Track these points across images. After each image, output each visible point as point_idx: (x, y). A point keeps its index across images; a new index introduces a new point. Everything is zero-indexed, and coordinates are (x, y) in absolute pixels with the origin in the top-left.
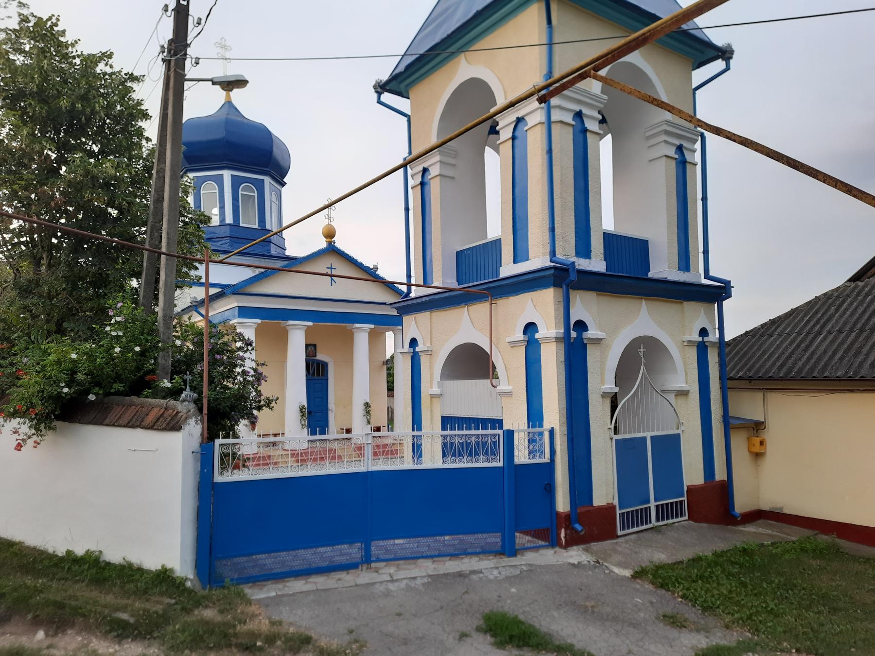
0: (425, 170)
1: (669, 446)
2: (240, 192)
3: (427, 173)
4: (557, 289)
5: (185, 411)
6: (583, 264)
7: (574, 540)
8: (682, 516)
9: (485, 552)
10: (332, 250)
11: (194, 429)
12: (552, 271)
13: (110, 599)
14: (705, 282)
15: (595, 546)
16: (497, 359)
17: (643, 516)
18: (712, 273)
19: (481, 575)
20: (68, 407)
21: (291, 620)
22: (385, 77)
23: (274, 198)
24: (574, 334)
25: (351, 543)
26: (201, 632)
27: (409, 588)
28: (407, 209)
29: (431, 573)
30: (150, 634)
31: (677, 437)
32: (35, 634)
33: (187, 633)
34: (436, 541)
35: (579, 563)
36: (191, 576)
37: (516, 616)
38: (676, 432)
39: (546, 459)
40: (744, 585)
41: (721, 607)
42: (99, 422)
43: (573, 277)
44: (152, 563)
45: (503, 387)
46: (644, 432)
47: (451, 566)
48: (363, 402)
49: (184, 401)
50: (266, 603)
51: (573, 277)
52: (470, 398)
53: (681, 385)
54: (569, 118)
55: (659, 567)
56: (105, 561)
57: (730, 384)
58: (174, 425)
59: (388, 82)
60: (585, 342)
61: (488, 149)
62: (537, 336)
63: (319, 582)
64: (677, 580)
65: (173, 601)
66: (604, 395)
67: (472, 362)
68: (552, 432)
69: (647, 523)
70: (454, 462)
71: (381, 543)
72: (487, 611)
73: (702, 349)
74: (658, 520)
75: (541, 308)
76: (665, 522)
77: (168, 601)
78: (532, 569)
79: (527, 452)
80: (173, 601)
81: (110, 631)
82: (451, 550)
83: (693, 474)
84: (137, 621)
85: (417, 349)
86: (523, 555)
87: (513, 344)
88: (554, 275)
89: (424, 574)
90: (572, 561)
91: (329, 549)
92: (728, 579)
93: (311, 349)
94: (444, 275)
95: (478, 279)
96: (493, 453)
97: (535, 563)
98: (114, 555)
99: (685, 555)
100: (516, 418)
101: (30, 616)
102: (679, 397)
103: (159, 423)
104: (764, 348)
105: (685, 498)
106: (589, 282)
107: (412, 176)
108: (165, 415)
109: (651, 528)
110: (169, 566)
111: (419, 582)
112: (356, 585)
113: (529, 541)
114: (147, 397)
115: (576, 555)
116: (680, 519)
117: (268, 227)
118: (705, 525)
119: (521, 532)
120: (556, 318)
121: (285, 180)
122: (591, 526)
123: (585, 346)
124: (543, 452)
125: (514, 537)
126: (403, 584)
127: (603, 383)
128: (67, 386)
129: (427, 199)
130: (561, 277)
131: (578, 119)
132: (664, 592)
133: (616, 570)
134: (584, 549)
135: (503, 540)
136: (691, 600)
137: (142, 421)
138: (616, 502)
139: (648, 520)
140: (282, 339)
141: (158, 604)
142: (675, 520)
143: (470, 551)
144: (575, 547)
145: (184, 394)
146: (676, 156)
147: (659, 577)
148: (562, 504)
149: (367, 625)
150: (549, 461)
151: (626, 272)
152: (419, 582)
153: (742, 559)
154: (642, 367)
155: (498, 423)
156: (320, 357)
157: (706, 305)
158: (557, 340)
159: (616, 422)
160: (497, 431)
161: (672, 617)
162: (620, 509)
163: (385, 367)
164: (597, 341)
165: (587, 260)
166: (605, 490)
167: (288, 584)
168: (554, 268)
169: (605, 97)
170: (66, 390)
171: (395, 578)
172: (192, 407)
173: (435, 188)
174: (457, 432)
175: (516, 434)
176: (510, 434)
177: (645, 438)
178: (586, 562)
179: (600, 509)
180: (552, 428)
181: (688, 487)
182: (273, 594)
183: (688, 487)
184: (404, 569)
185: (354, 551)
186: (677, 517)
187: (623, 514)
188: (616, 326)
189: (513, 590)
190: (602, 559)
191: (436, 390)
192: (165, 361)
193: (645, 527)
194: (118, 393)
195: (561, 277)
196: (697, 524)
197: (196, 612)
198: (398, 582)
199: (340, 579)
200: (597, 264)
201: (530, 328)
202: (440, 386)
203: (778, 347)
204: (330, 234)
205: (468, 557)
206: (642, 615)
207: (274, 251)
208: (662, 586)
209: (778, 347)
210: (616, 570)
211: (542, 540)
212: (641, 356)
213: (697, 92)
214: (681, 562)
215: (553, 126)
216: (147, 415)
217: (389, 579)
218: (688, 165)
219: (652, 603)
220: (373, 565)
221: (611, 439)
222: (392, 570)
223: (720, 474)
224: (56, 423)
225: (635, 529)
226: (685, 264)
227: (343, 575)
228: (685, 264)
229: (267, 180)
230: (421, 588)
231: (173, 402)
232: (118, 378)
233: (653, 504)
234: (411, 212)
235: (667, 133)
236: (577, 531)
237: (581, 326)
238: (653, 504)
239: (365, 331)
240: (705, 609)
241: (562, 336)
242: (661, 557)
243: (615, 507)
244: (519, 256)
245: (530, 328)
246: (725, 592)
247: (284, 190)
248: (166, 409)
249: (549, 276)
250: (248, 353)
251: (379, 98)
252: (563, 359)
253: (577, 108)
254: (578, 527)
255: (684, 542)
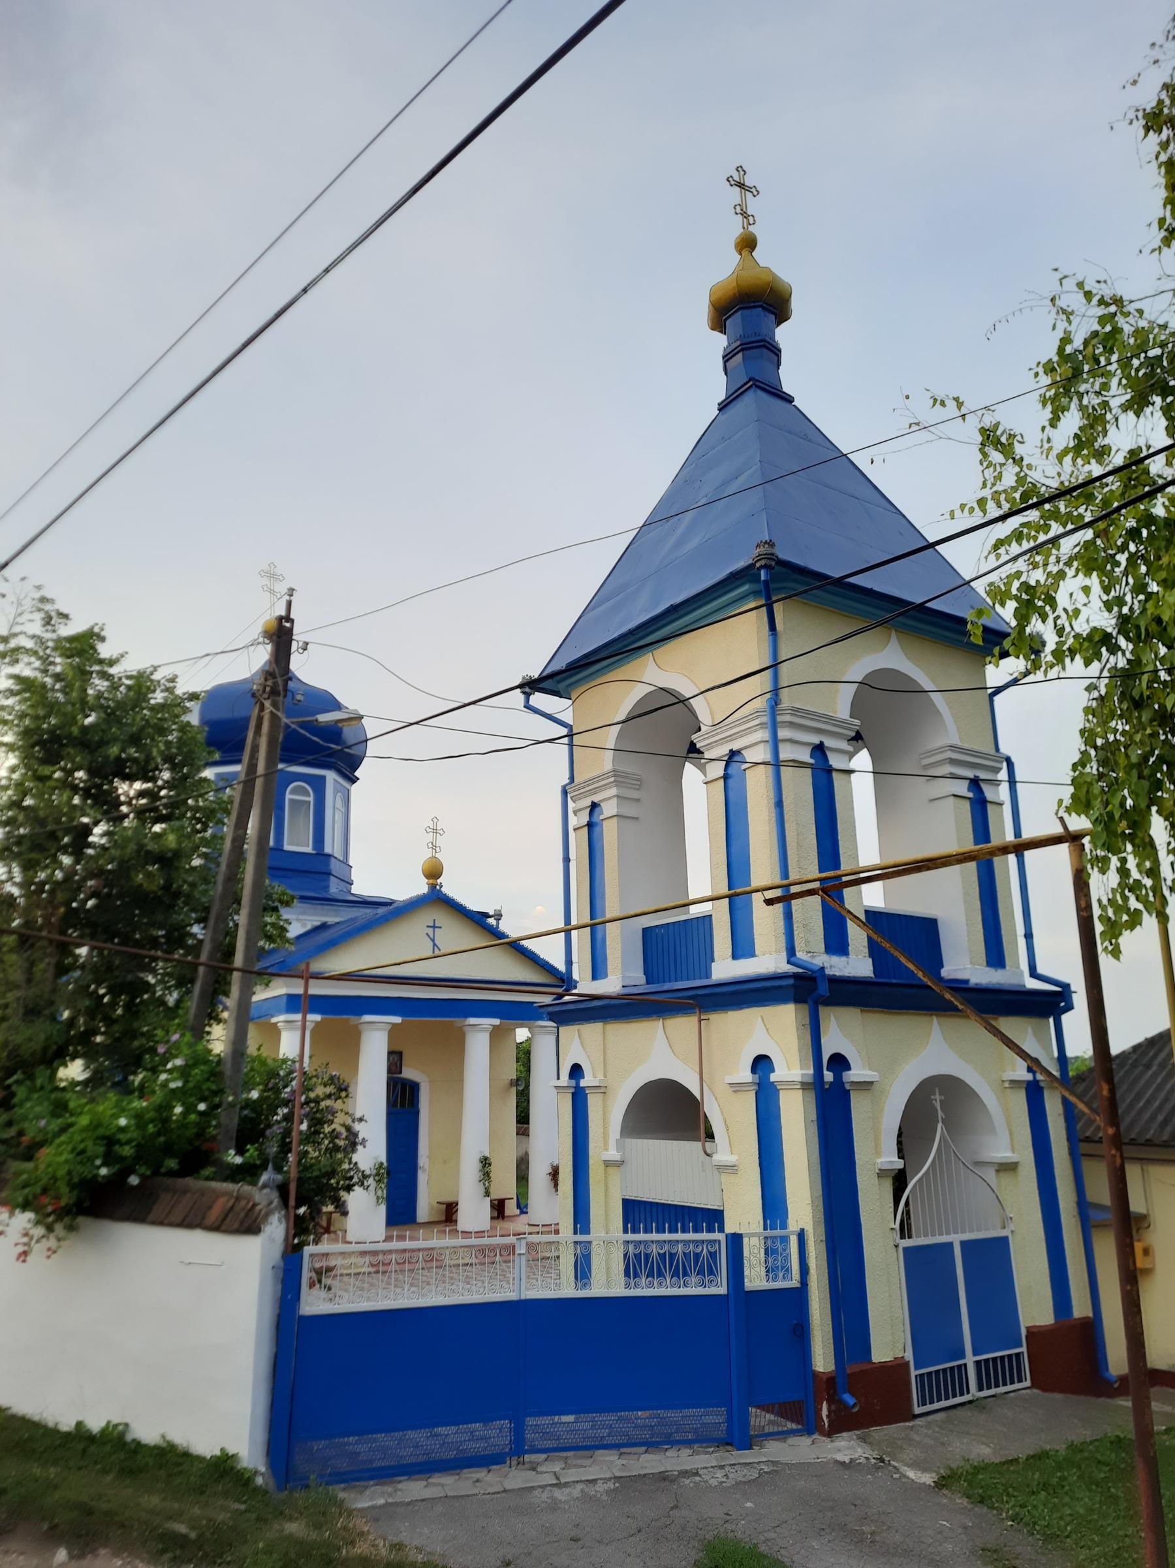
0: (594, 806)
1: (990, 1257)
2: (288, 796)
3: (597, 810)
4: (800, 1006)
5: (264, 1203)
6: (838, 966)
7: (841, 1423)
8: (1020, 1381)
9: (701, 1440)
10: (437, 899)
11: (276, 1229)
12: (791, 981)
13: (154, 1501)
14: (1032, 984)
15: (879, 1433)
16: (712, 1110)
17: (955, 1380)
18: (1040, 970)
19: (697, 1479)
20: (103, 1195)
21: (415, 1543)
22: (536, 674)
23: (339, 803)
24: (828, 1076)
25: (486, 1421)
26: (293, 1556)
27: (586, 1498)
28: (567, 860)
29: (618, 1474)
30: (221, 1556)
31: (1004, 1241)
32: (54, 1555)
33: (275, 1556)
34: (620, 1419)
35: (852, 1460)
36: (263, 1469)
37: (756, 1545)
38: (1003, 1233)
39: (794, 1282)
40: (1114, 1499)
41: (1074, 1536)
42: (140, 1217)
43: (823, 989)
44: (205, 1446)
45: (723, 1154)
46: (948, 1233)
47: (650, 1463)
48: (480, 1155)
49: (265, 1186)
50: (375, 1515)
51: (823, 989)
52: (667, 1171)
53: (1002, 1152)
54: (805, 756)
55: (978, 1469)
56: (134, 1440)
57: (1084, 1148)
58: (250, 1226)
59: (542, 679)
60: (848, 1087)
61: (688, 767)
62: (773, 1077)
63: (446, 1484)
64: (1006, 1490)
65: (243, 1507)
66: (882, 1174)
67: (670, 1111)
68: (801, 1235)
69: (962, 1394)
70: (651, 1285)
71: (540, 1421)
72: (709, 1537)
73: (1034, 1092)
74: (980, 1389)
75: (776, 1032)
76: (992, 1391)
77: (237, 1506)
78: (777, 1469)
79: (763, 1269)
80: (243, 1507)
81: (163, 1551)
82: (646, 1434)
83: (1034, 1307)
84: (200, 1536)
85: (583, 1083)
86: (762, 1447)
87: (737, 1087)
88: (794, 986)
89: (608, 1475)
90: (840, 1457)
91: (453, 1429)
92: (1090, 1490)
93: (395, 1060)
94: (625, 967)
95: (675, 977)
96: (711, 1273)
97: (782, 1459)
98: (147, 1432)
99: (1021, 1449)
100: (743, 1213)
101: (45, 1526)
102: (1001, 1174)
103: (227, 1221)
104: (1137, 1089)
105: (1024, 1349)
106: (847, 993)
107: (575, 813)
108: (237, 1209)
109: (970, 1402)
110: (231, 1451)
111: (601, 1487)
112: (505, 1491)
113: (770, 1422)
114: (207, 1179)
115: (846, 1448)
116: (1017, 1386)
117: (328, 849)
118: (1059, 1396)
119: (758, 1407)
120: (800, 1051)
121: (356, 774)
122: (869, 1397)
123: (846, 1095)
124: (788, 1270)
125: (746, 1417)
126: (576, 1491)
127: (878, 1152)
128: (104, 1164)
129: (597, 848)
130: (807, 990)
131: (818, 754)
132: (985, 1509)
133: (911, 1474)
134: (859, 1438)
135: (730, 1420)
136: (1027, 1525)
137: (203, 1218)
138: (909, 1356)
139: (964, 1389)
140: (351, 1044)
141: (224, 1510)
142: (1010, 1388)
143: (678, 1437)
144: (844, 1434)
145: (264, 1177)
146: (970, 795)
147: (970, 1483)
148: (822, 1359)
149: (530, 1554)
150: (798, 1285)
151: (905, 974)
152: (601, 1487)
153: (1113, 1456)
154: (940, 1125)
155: (714, 1218)
156: (408, 1073)
157: (1034, 1021)
158: (804, 1086)
159: (907, 1204)
160: (717, 1236)
161: (995, 1551)
162: (916, 1368)
163: (514, 1090)
164: (866, 1086)
165: (843, 959)
166: (890, 1338)
167: (400, 1486)
168: (795, 976)
169: (857, 722)
170: (104, 1171)
171: (563, 1481)
172: (275, 1197)
173: (610, 833)
174: (655, 1236)
175: (745, 1240)
176: (736, 1240)
177: (951, 1245)
178: (862, 1460)
179: (883, 1366)
180: (802, 1230)
181: (1028, 1329)
182: (381, 1501)
183: (1028, 1329)
184: (576, 1466)
185: (497, 1433)
186: (1012, 1383)
187: (922, 1375)
188: (891, 1061)
189: (749, 1504)
190: (888, 1454)
191: (613, 1154)
192: (229, 1120)
193: (959, 1400)
194: (171, 1174)
195: (807, 990)
196: (1047, 1395)
197: (276, 1526)
198: (570, 1483)
199: (478, 1481)
200: (857, 964)
201: (761, 1063)
202: (620, 1147)
203: (1160, 1088)
204: (433, 873)
205: (676, 1448)
206: (950, 1547)
207: (334, 889)
208: (982, 1501)
209: (1160, 1088)
210: (911, 1474)
211: (792, 1421)
212: (934, 1109)
213: (996, 699)
214: (1015, 1461)
215: (786, 772)
216: (210, 1207)
217: (555, 1482)
218: (989, 807)
219: (966, 1528)
220: (527, 1458)
221: (896, 1246)
222: (557, 1467)
223: (1081, 1308)
224: (81, 1220)
225: (944, 1404)
226: (996, 955)
227: (481, 1474)
228: (996, 955)
229: (331, 776)
230: (605, 1498)
231: (247, 1188)
232: (169, 1150)
233: (970, 1360)
234: (573, 865)
235: (952, 762)
236: (847, 1408)
237: (839, 1062)
238: (970, 1360)
239: (485, 1030)
240: (1049, 1538)
241: (810, 1080)
242: (984, 1452)
243: (907, 1363)
244: (742, 947)
245: (761, 1063)
246: (1081, 1511)
247: (355, 788)
248: (238, 1199)
249: (787, 986)
250: (339, 1101)
251: (527, 700)
252: (814, 1117)
253: (816, 740)
254: (850, 1399)
255: (1020, 1425)
